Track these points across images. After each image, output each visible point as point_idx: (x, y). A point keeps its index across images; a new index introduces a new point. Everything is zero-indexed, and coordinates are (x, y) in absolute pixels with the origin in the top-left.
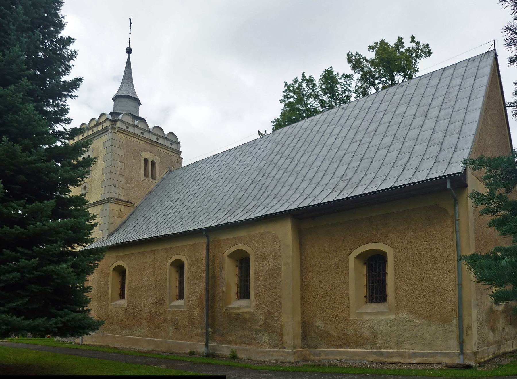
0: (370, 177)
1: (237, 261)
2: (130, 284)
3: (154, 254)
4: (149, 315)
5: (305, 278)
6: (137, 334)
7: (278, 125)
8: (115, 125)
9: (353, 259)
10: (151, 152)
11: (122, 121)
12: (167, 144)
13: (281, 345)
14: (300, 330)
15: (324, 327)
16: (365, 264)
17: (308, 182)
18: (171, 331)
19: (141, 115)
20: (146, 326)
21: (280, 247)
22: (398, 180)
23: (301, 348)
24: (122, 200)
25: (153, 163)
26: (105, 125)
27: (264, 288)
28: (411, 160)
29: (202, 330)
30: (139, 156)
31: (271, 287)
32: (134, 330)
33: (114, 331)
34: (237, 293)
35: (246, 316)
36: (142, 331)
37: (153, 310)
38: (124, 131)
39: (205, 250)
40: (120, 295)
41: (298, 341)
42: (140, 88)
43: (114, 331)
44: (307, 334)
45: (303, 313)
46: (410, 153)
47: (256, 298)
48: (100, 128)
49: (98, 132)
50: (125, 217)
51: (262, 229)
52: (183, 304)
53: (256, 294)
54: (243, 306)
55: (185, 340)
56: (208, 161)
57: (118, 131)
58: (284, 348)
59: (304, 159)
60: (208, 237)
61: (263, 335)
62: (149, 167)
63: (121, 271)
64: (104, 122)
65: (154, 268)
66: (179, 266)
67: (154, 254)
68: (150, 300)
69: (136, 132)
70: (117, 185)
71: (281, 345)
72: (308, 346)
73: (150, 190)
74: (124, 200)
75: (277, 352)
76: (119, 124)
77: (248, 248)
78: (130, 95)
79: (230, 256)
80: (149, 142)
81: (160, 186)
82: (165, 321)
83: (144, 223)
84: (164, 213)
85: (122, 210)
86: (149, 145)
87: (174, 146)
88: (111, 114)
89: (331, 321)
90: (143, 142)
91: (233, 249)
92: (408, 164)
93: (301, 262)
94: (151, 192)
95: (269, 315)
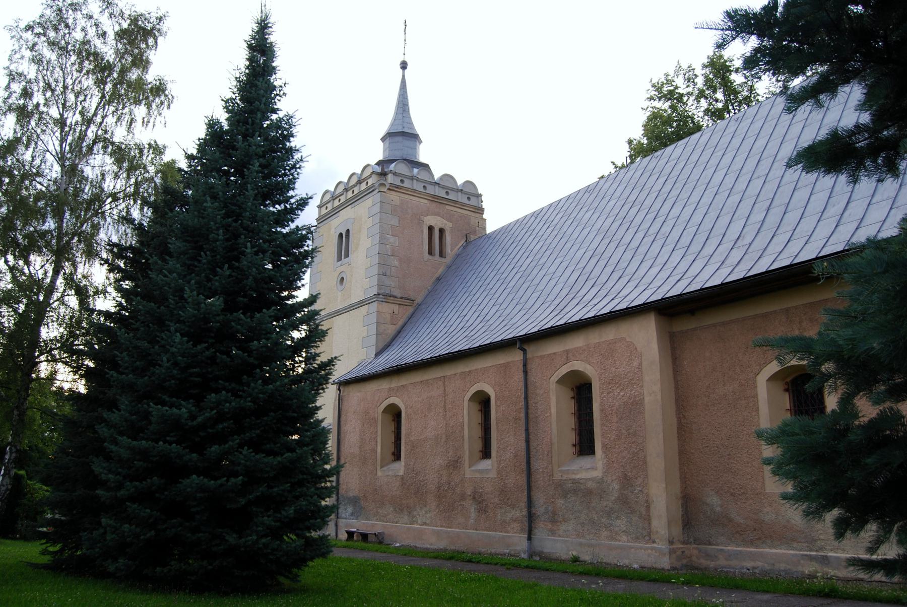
0: (782, 238)
1: (572, 389)
2: (408, 435)
3: (444, 383)
4: (439, 488)
5: (684, 416)
6: (419, 522)
7: (638, 151)
8: (386, 180)
9: (765, 383)
10: (438, 214)
11: (395, 174)
12: (463, 199)
13: (649, 536)
14: (680, 513)
15: (722, 506)
16: (787, 390)
17: (683, 251)
18: (473, 514)
19: (423, 158)
20: (433, 507)
21: (640, 364)
22: (829, 243)
23: (684, 543)
24: (395, 297)
25: (441, 231)
26: (370, 182)
27: (617, 436)
28: (851, 205)
29: (521, 511)
30: (421, 222)
31: (629, 434)
32: (415, 513)
33: (385, 516)
34: (574, 445)
35: (590, 485)
36: (428, 516)
37: (445, 479)
38: (397, 187)
39: (522, 373)
40: (393, 454)
41: (677, 531)
42: (420, 123)
43: (385, 516)
44: (691, 515)
45: (684, 479)
46: (849, 194)
47: (604, 452)
48: (363, 186)
49: (360, 192)
50: (400, 323)
51: (609, 333)
52: (490, 467)
53: (604, 446)
54: (589, 470)
55: (496, 531)
56: (525, 222)
57: (389, 189)
58: (654, 542)
59: (676, 211)
60: (524, 351)
61: (618, 518)
62: (436, 239)
63: (395, 414)
64: (370, 176)
65: (445, 407)
66: (483, 402)
67: (444, 383)
68: (439, 461)
69: (415, 188)
70: (388, 274)
71: (649, 536)
72: (697, 541)
73: (437, 275)
74: (399, 295)
75: (641, 548)
76: (390, 178)
77: (588, 367)
78: (406, 130)
79: (561, 381)
80: (435, 199)
81: (453, 267)
82: (463, 497)
83: (471, 304)
84: (458, 314)
85: (396, 312)
86: (434, 204)
87: (473, 202)
88: (379, 163)
89: (732, 494)
90: (426, 201)
91: (564, 370)
92: (846, 214)
93: (677, 388)
94: (438, 279)
95: (626, 481)
